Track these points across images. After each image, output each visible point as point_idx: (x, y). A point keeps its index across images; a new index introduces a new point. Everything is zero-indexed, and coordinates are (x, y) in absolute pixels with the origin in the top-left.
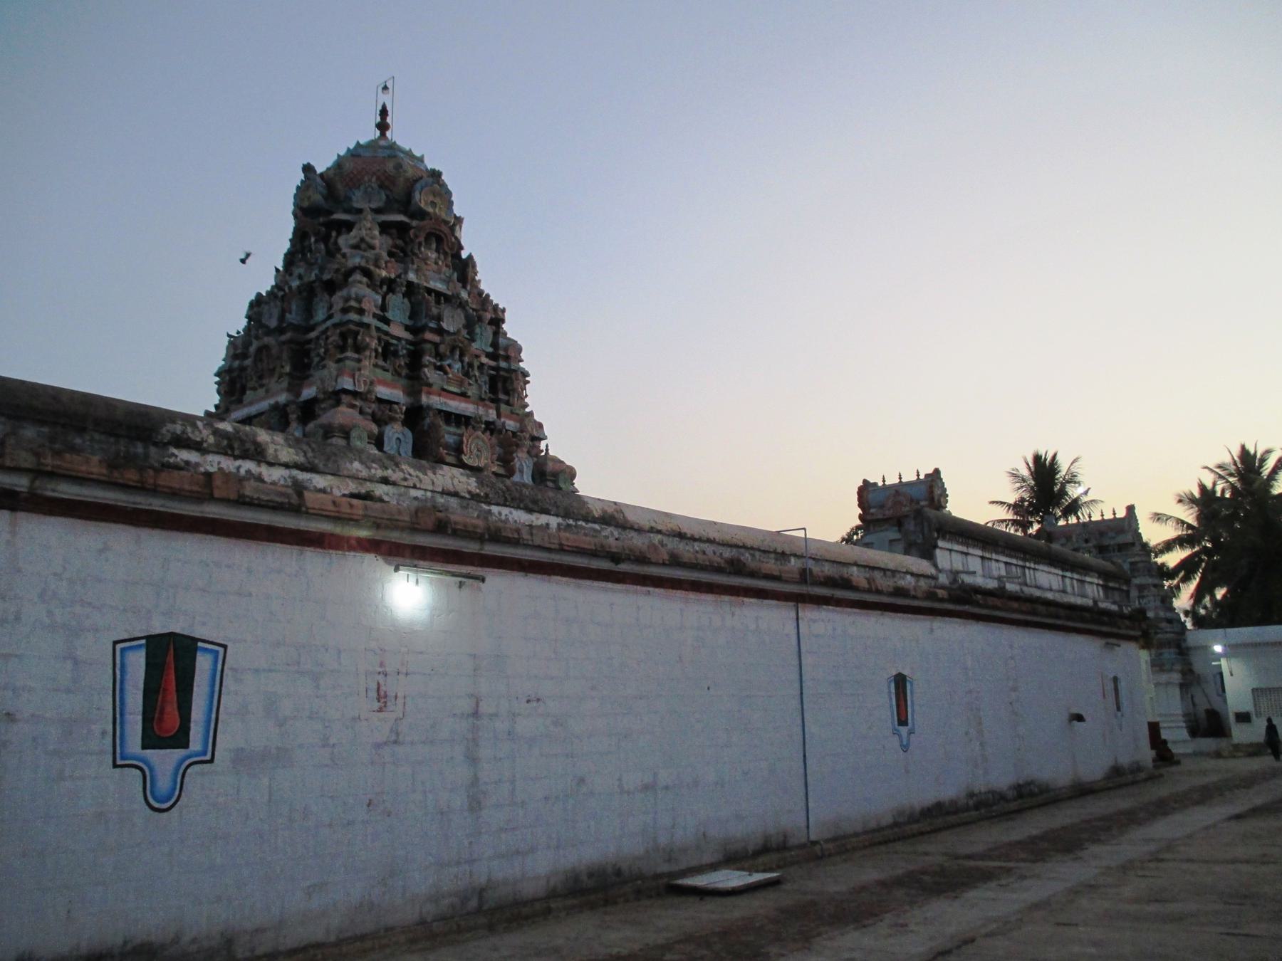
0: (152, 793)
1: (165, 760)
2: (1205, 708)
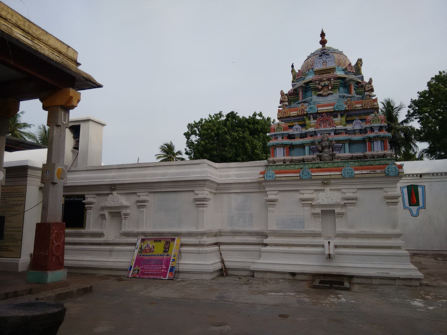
0: (415, 215)
1: (414, 209)
2: (416, 99)
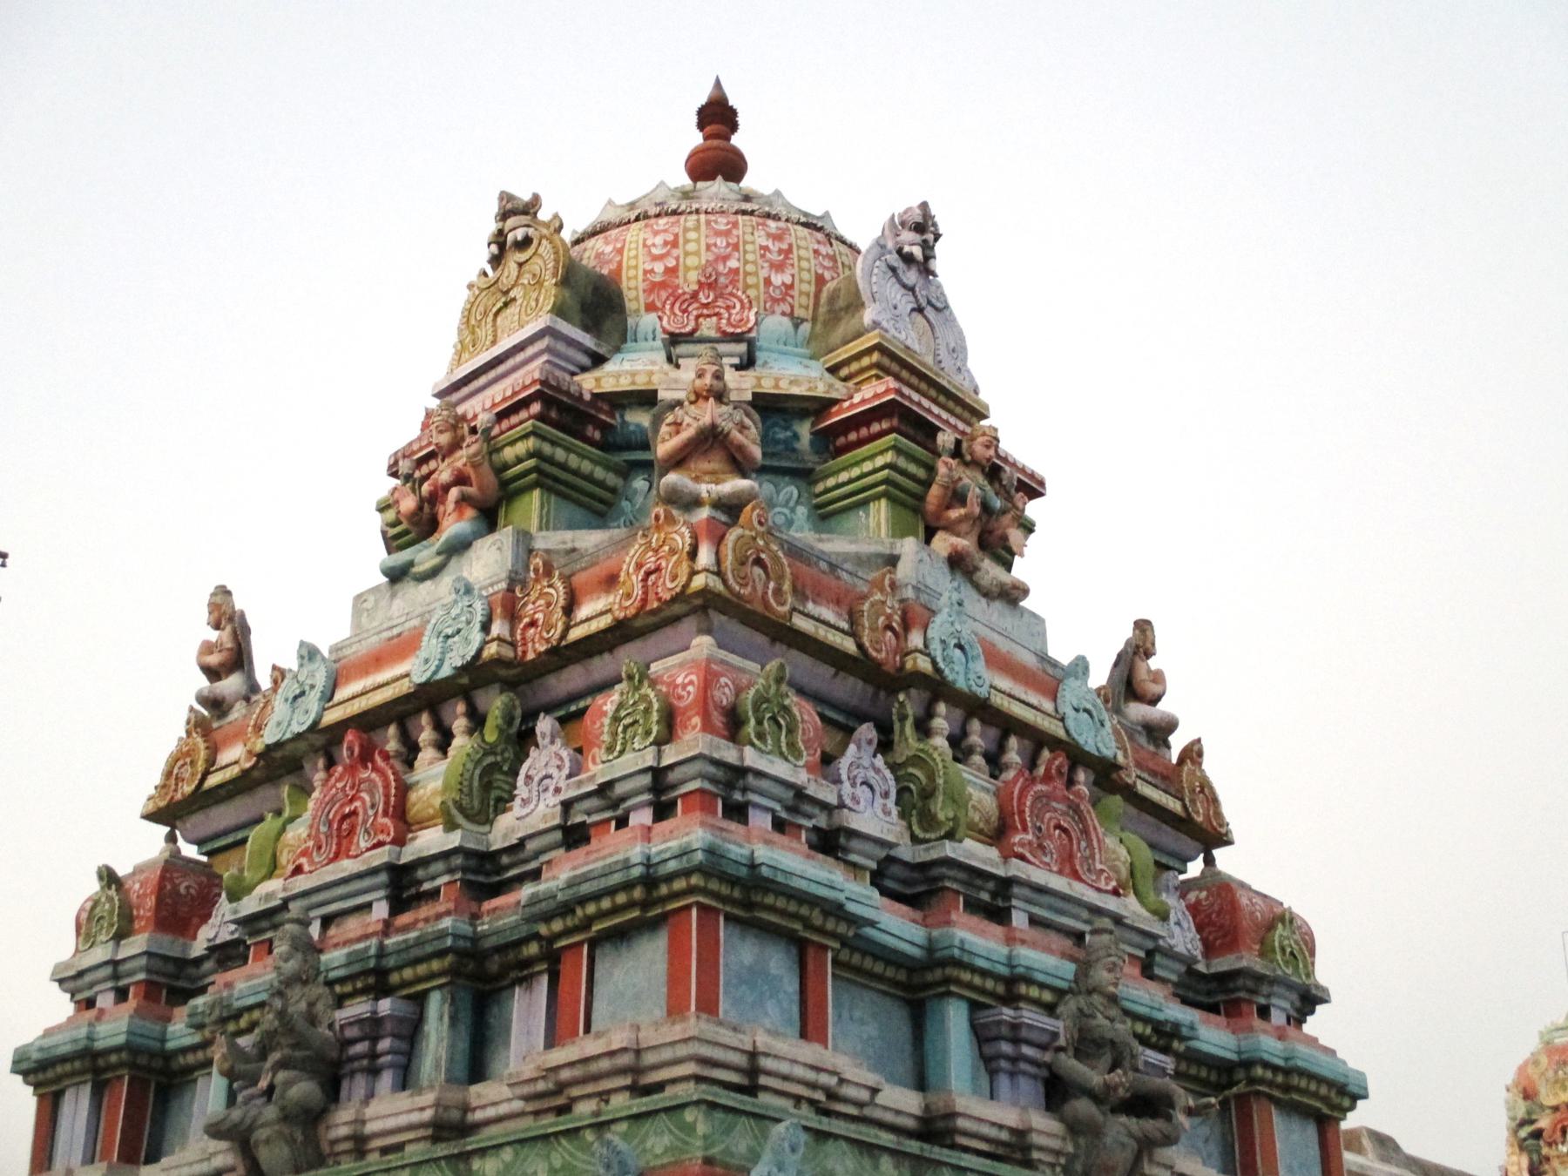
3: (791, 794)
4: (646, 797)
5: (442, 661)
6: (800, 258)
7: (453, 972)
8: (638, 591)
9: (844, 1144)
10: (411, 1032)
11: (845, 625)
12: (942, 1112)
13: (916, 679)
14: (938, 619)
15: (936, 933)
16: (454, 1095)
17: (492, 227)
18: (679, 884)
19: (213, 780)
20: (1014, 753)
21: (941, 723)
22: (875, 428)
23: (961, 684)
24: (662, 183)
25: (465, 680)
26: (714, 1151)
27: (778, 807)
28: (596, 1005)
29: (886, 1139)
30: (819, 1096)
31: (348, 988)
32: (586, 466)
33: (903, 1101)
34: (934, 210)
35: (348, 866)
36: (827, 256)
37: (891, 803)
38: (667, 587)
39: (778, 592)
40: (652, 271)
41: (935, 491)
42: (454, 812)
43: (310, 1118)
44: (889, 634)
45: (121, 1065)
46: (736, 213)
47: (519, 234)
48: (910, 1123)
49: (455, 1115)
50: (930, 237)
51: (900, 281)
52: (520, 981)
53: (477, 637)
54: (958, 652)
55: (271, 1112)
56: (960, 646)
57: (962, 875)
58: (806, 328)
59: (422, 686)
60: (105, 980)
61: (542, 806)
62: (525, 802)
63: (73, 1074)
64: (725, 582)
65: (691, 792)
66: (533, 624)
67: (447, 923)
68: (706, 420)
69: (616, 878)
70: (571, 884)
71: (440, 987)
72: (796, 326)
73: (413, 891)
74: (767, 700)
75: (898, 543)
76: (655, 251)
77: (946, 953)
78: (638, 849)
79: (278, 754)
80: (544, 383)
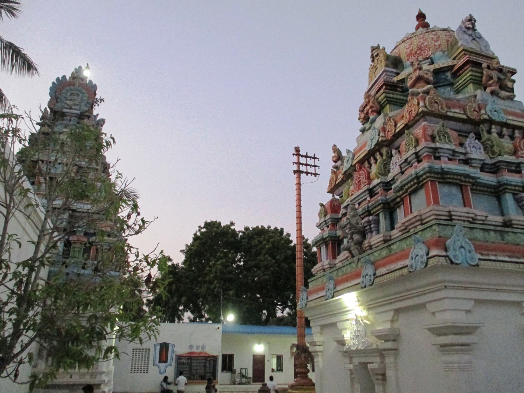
1: (162, 365)
3: (451, 152)
4: (415, 160)
5: (372, 145)
6: (442, 38)
7: (383, 208)
8: (408, 117)
9: (478, 230)
10: (377, 222)
11: (463, 112)
12: (508, 220)
13: (484, 121)
14: (488, 106)
15: (499, 178)
16: (387, 234)
17: (370, 54)
18: (424, 177)
19: (337, 182)
20: (517, 134)
21: (494, 129)
22: (466, 68)
23: (498, 119)
24: (407, 33)
25: (377, 147)
26: (441, 235)
27: (448, 155)
28: (412, 208)
29: (492, 228)
30: (471, 220)
31: (363, 216)
32: (398, 97)
33: (499, 219)
34: (473, 15)
35: (361, 191)
36: (449, 35)
37: (482, 151)
38: (414, 113)
39: (442, 108)
40: (407, 52)
41: (484, 79)
42: (378, 175)
43: (360, 243)
44: (475, 112)
45: (329, 240)
46: (425, 33)
47: (376, 54)
48: (501, 224)
49: (389, 238)
50: (473, 22)
51: (467, 34)
52: (398, 207)
53: (377, 137)
54: (495, 113)
55: (353, 244)
56: (495, 111)
57: (505, 164)
58: (446, 53)
59: (369, 151)
60: (324, 225)
61: (396, 169)
62: (393, 169)
63: (321, 244)
64: (427, 108)
65: (426, 156)
66: (389, 131)
67: (379, 198)
68: (417, 74)
69: (410, 178)
70: (401, 182)
71: (381, 212)
72: (444, 53)
73: (374, 194)
74: (441, 131)
75: (476, 92)
76: (407, 47)
77: (503, 182)
78: (413, 171)
79: (347, 173)
80: (384, 81)
